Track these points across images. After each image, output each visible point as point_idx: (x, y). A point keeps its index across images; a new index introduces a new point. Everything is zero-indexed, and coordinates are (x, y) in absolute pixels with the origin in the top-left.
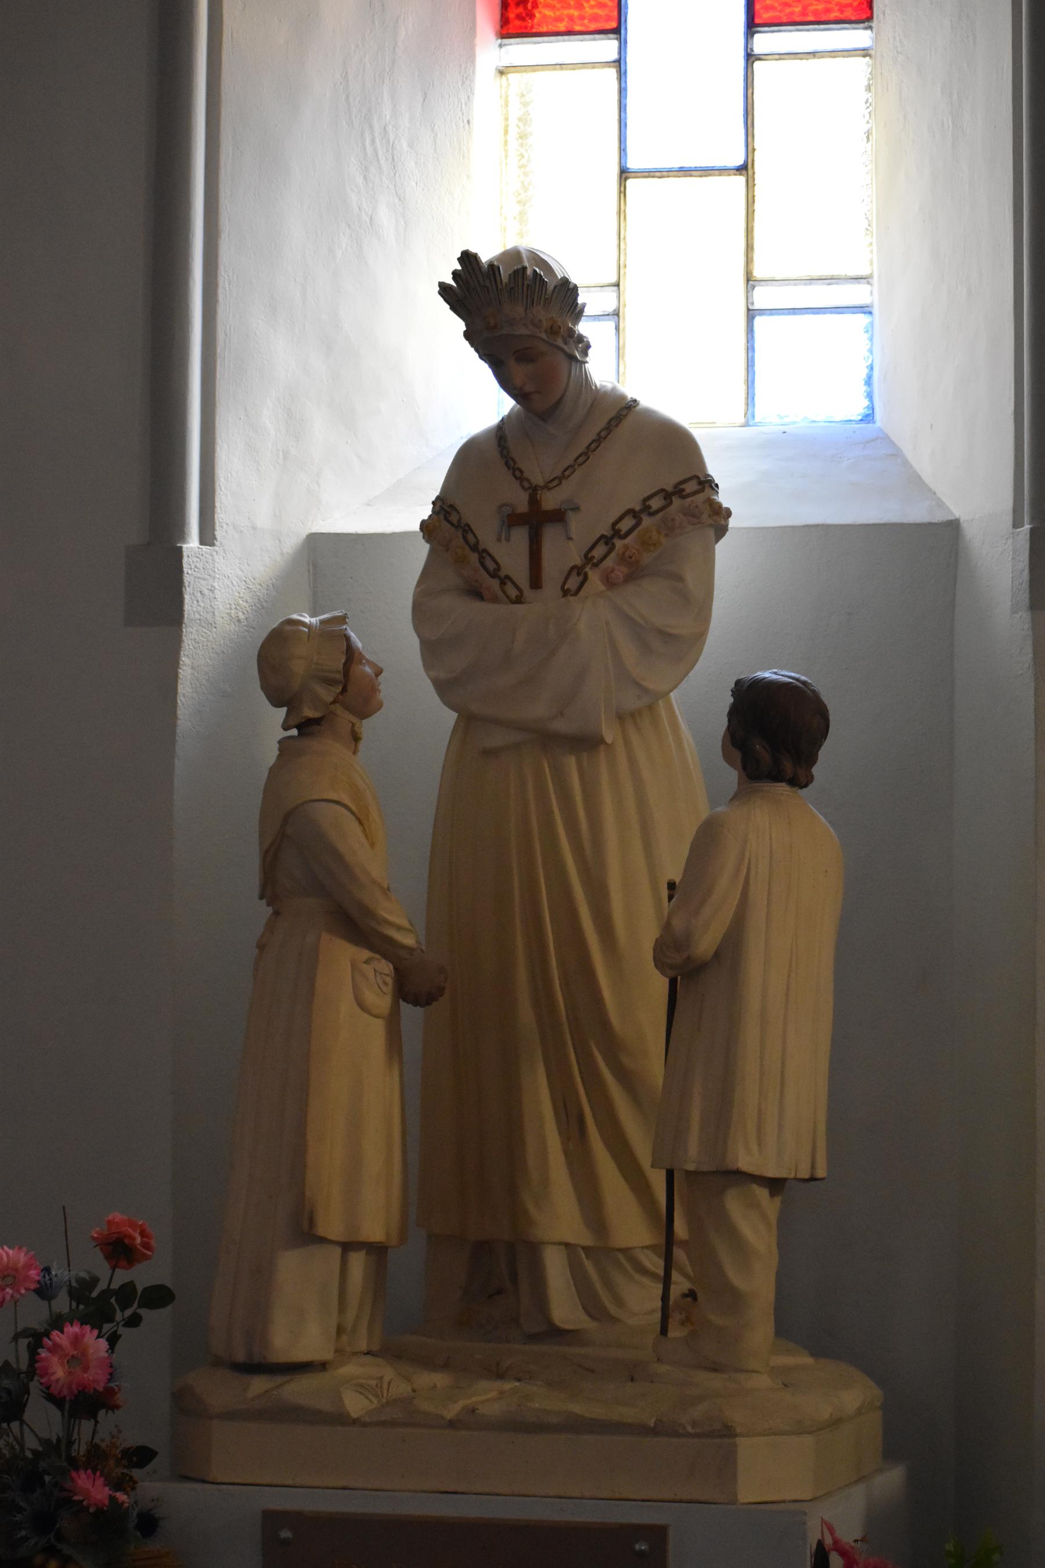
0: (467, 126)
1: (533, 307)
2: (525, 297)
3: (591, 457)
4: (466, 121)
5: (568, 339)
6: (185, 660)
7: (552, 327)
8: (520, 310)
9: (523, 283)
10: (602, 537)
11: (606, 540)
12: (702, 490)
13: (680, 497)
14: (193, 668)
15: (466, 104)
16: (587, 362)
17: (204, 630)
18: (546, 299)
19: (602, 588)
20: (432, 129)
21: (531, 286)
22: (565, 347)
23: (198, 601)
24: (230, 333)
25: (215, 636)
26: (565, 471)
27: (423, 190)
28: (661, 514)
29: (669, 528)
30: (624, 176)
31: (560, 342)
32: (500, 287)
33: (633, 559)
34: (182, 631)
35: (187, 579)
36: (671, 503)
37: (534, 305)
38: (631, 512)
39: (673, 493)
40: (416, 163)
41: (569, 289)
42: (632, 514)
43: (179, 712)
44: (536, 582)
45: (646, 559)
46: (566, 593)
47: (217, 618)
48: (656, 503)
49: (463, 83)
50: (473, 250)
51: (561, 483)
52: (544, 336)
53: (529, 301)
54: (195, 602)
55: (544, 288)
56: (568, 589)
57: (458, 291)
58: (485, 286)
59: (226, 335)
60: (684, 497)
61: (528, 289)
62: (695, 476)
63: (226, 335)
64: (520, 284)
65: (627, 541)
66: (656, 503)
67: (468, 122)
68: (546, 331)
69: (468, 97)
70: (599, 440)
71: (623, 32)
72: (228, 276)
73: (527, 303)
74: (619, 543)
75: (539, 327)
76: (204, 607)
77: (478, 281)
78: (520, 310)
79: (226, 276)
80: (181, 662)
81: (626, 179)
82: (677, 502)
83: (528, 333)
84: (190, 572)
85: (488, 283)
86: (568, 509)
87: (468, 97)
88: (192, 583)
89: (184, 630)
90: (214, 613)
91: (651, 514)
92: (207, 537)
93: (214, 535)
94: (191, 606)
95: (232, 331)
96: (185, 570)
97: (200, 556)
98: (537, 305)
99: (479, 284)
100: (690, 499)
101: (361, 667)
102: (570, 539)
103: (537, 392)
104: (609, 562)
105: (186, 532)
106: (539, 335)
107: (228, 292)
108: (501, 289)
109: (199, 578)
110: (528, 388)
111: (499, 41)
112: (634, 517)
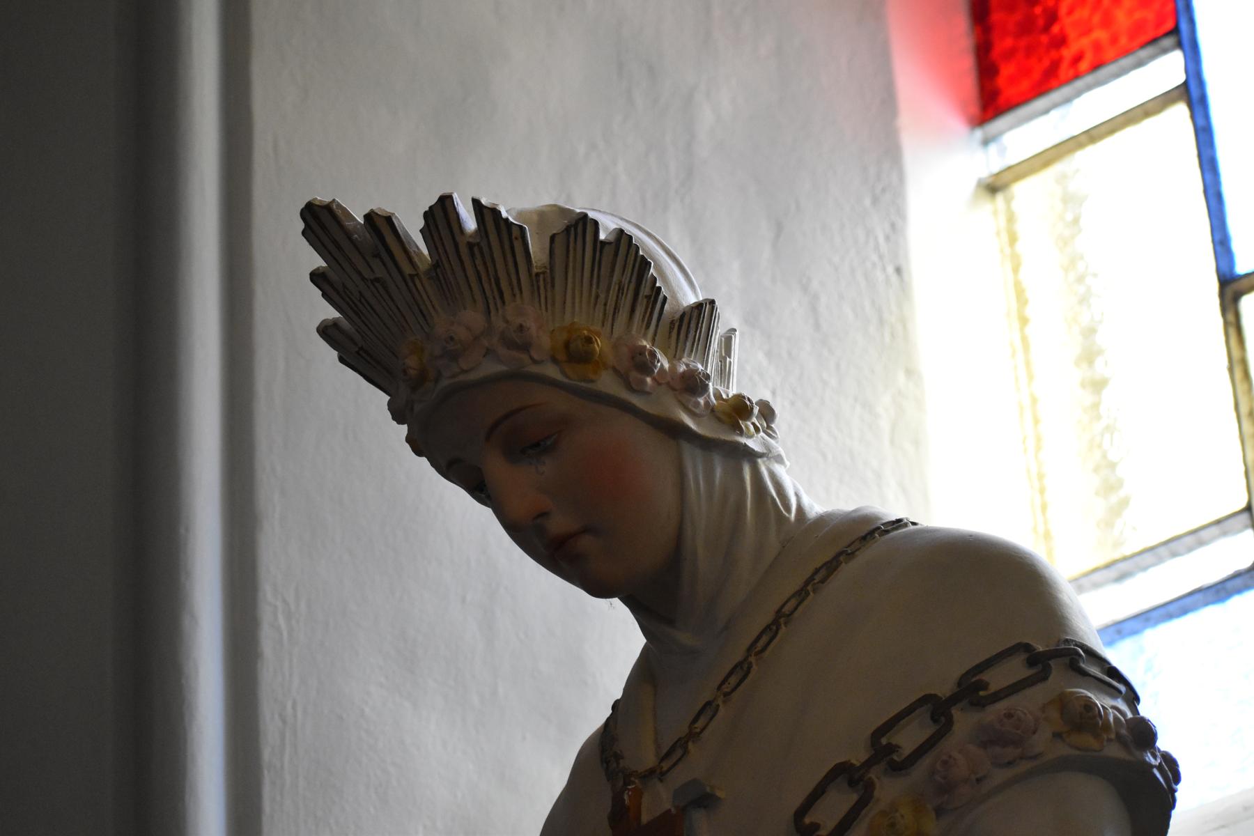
0: (894, 278)
1: (504, 303)
2: (474, 285)
3: (755, 667)
4: (890, 269)
7: (567, 345)
8: (472, 317)
12: (1043, 677)
13: (972, 704)
15: (887, 238)
16: (767, 454)
18: (537, 275)
20: (805, 289)
21: (478, 244)
22: (636, 401)
24: (295, 716)
26: (695, 720)
27: (792, 404)
28: (926, 761)
30: (1229, 291)
31: (607, 383)
32: (407, 270)
36: (950, 723)
37: (507, 295)
38: (842, 773)
39: (954, 699)
40: (769, 354)
41: (600, 246)
49: (875, 201)
50: (323, 197)
51: (686, 752)
52: (552, 371)
53: (486, 286)
55: (518, 245)
57: (345, 324)
58: (377, 280)
59: (284, 722)
60: (980, 704)
61: (472, 255)
62: (1019, 644)
63: (284, 722)
66: (908, 738)
67: (898, 271)
68: (554, 360)
69: (893, 226)
70: (772, 629)
71: (1184, 26)
72: (285, 601)
77: (360, 273)
78: (472, 317)
79: (279, 604)
81: (1237, 298)
82: (964, 721)
83: (501, 368)
85: (380, 272)
87: (893, 226)
95: (299, 714)
99: (363, 279)
100: (1002, 706)
103: (585, 530)
106: (534, 369)
107: (285, 634)
108: (411, 276)
110: (559, 524)
111: (979, 134)
112: (852, 783)
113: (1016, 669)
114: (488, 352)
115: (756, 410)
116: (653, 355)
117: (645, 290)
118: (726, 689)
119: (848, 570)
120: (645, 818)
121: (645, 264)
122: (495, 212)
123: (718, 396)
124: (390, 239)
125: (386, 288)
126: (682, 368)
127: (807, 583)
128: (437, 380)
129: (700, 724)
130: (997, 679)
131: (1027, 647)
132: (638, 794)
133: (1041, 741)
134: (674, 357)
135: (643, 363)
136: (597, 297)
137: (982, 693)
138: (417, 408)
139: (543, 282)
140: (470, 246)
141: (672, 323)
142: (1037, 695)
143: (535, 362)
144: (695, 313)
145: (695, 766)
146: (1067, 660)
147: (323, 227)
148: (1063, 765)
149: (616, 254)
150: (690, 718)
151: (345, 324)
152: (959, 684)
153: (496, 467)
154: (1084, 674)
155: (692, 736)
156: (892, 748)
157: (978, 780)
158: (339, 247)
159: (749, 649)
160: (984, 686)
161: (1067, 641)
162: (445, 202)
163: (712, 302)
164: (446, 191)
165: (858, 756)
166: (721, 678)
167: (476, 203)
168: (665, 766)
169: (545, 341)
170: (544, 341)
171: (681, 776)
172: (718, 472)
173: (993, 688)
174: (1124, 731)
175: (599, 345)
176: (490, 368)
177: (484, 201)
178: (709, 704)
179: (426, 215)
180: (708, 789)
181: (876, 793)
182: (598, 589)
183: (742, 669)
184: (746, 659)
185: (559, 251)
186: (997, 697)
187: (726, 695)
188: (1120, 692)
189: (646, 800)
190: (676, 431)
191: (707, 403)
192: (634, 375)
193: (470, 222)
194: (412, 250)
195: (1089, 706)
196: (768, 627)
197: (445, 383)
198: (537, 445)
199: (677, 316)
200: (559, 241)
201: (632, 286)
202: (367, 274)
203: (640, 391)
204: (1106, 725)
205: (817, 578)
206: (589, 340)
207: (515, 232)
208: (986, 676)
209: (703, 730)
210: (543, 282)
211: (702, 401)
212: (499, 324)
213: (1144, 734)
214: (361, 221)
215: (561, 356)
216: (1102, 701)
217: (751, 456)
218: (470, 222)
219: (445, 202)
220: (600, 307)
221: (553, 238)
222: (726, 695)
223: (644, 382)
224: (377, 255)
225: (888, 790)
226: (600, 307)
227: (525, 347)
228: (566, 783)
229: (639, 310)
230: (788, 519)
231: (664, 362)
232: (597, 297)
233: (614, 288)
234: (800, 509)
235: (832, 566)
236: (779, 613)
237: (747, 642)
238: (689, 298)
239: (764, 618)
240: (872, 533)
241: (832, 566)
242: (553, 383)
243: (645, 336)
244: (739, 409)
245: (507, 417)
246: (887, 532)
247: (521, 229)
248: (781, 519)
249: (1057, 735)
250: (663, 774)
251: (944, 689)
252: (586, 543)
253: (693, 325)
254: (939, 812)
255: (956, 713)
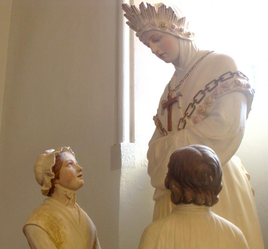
5: (172, 29)
6: (122, 179)
7: (161, 25)
9: (144, 10)
10: (190, 104)
11: (192, 105)
12: (232, 77)
14: (126, 182)
17: (130, 169)
18: (157, 14)
19: (193, 124)
22: (172, 33)
23: (127, 160)
25: (135, 171)
28: (214, 90)
29: (215, 96)
31: (168, 31)
32: (137, 13)
33: (203, 110)
34: (121, 170)
35: (122, 154)
38: (201, 91)
39: (218, 80)
41: (166, 9)
42: (201, 93)
43: (120, 196)
44: (170, 129)
45: (209, 110)
46: (179, 130)
47: (135, 165)
48: (211, 86)
51: (179, 87)
52: (159, 29)
54: (126, 161)
55: (154, 10)
56: (180, 129)
58: (133, 16)
59: (137, 79)
60: (222, 81)
61: (147, 11)
63: (137, 79)
64: (143, 10)
65: (201, 103)
66: (211, 86)
68: (159, 27)
73: (149, 18)
74: (197, 106)
75: (155, 25)
76: (130, 162)
78: (147, 21)
80: (121, 180)
82: (220, 83)
84: (124, 151)
85: (133, 14)
86: (178, 96)
88: (125, 154)
89: (122, 170)
90: (134, 164)
91: (209, 91)
92: (132, 140)
93: (134, 139)
94: (124, 161)
96: (122, 151)
97: (128, 146)
98: (153, 17)
100: (226, 81)
101: (67, 168)
102: (179, 108)
103: (165, 53)
104: (195, 114)
105: (123, 139)
109: (127, 153)
112: (202, 93)
113: (228, 76)
114: (149, 26)
115: (192, 34)
116: (175, 26)
117: (174, 16)
118: (185, 77)
119: (204, 59)
120: (173, 97)
121: (174, 12)
122: (150, 5)
123: (186, 32)
124: (134, 9)
125: (134, 17)
126: (180, 28)
127: (198, 61)
128: (142, 30)
129: (181, 83)
130: (225, 77)
131: (230, 72)
132: (172, 94)
133: (231, 87)
134: (179, 26)
135: (173, 27)
136: (166, 17)
137: (223, 79)
138: (140, 35)
139: (157, 15)
140: (146, 10)
141: (178, 21)
142: (232, 79)
143: (156, 28)
144: (182, 19)
145: (178, 91)
146: (237, 74)
147: (125, 8)
148: (235, 91)
149: (169, 10)
150: (180, 82)
151: (129, 22)
152: (219, 78)
153: (151, 43)
154: (239, 76)
155: (180, 85)
156: (208, 88)
157: (221, 93)
158: (127, 10)
159: (189, 71)
160: (223, 78)
161: (237, 71)
162: (142, 3)
163: (185, 17)
164: (142, 2)
165: (203, 89)
166: (184, 76)
167: (147, 3)
168: (176, 89)
169: (158, 24)
170: (158, 24)
171: (178, 91)
172: (185, 44)
173: (225, 79)
174: (245, 86)
175: (166, 25)
176: (149, 29)
177: (148, 3)
178: (182, 80)
179: (140, 5)
180: (181, 94)
181: (206, 95)
182: (167, 62)
183: (188, 75)
184: (188, 73)
185: (160, 10)
186: (225, 80)
187: (185, 79)
188: (245, 79)
189: (173, 94)
190: (178, 38)
191: (184, 33)
192: (172, 29)
193: (146, 6)
194: (138, 11)
195: (239, 82)
196: (192, 68)
197: (143, 31)
198: (157, 40)
199: (179, 19)
200: (160, 9)
201: (172, 16)
202: (132, 15)
203: (172, 31)
204: (242, 85)
205: (200, 60)
206: (164, 24)
207: (153, 8)
208: (224, 77)
209: (182, 84)
210: (157, 15)
211: (183, 33)
212: (151, 22)
213: (248, 86)
214: (130, 6)
215: (160, 27)
216: (241, 81)
217: (191, 41)
218: (146, 6)
219: (142, 3)
220: (167, 18)
221: (159, 8)
222: (185, 79)
223: (173, 30)
224: (133, 12)
225: (208, 94)
226: (167, 18)
227: (155, 25)
228: (163, 92)
229: (173, 19)
230: (196, 51)
231: (176, 27)
232: (166, 17)
233: (169, 16)
234: (199, 50)
235: (202, 58)
236: (194, 66)
237: (189, 70)
238: (181, 17)
239: (192, 66)
240: (209, 53)
241: (202, 58)
242: (159, 31)
243: (174, 23)
244: (189, 34)
245: (152, 36)
246: (211, 53)
247: (154, 7)
248: (195, 51)
249: (234, 86)
250: (176, 91)
251: (217, 79)
252: (165, 55)
253: (182, 21)
254: (215, 98)
255: (219, 82)
